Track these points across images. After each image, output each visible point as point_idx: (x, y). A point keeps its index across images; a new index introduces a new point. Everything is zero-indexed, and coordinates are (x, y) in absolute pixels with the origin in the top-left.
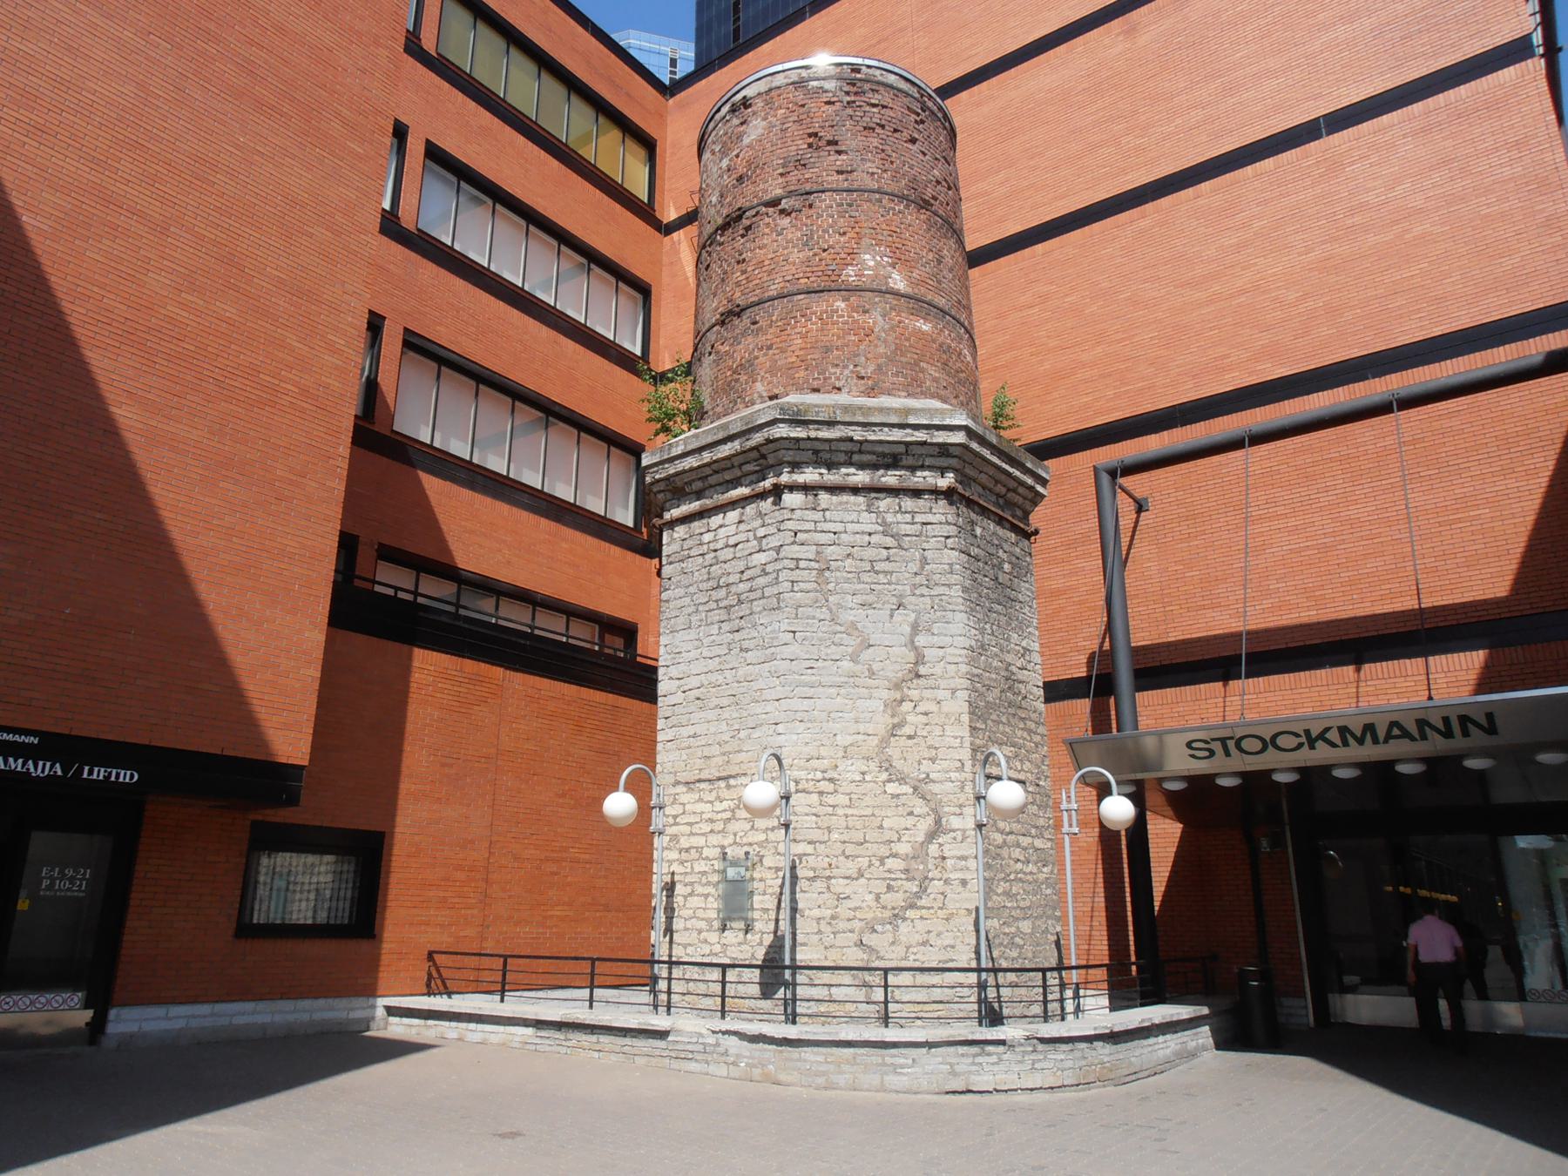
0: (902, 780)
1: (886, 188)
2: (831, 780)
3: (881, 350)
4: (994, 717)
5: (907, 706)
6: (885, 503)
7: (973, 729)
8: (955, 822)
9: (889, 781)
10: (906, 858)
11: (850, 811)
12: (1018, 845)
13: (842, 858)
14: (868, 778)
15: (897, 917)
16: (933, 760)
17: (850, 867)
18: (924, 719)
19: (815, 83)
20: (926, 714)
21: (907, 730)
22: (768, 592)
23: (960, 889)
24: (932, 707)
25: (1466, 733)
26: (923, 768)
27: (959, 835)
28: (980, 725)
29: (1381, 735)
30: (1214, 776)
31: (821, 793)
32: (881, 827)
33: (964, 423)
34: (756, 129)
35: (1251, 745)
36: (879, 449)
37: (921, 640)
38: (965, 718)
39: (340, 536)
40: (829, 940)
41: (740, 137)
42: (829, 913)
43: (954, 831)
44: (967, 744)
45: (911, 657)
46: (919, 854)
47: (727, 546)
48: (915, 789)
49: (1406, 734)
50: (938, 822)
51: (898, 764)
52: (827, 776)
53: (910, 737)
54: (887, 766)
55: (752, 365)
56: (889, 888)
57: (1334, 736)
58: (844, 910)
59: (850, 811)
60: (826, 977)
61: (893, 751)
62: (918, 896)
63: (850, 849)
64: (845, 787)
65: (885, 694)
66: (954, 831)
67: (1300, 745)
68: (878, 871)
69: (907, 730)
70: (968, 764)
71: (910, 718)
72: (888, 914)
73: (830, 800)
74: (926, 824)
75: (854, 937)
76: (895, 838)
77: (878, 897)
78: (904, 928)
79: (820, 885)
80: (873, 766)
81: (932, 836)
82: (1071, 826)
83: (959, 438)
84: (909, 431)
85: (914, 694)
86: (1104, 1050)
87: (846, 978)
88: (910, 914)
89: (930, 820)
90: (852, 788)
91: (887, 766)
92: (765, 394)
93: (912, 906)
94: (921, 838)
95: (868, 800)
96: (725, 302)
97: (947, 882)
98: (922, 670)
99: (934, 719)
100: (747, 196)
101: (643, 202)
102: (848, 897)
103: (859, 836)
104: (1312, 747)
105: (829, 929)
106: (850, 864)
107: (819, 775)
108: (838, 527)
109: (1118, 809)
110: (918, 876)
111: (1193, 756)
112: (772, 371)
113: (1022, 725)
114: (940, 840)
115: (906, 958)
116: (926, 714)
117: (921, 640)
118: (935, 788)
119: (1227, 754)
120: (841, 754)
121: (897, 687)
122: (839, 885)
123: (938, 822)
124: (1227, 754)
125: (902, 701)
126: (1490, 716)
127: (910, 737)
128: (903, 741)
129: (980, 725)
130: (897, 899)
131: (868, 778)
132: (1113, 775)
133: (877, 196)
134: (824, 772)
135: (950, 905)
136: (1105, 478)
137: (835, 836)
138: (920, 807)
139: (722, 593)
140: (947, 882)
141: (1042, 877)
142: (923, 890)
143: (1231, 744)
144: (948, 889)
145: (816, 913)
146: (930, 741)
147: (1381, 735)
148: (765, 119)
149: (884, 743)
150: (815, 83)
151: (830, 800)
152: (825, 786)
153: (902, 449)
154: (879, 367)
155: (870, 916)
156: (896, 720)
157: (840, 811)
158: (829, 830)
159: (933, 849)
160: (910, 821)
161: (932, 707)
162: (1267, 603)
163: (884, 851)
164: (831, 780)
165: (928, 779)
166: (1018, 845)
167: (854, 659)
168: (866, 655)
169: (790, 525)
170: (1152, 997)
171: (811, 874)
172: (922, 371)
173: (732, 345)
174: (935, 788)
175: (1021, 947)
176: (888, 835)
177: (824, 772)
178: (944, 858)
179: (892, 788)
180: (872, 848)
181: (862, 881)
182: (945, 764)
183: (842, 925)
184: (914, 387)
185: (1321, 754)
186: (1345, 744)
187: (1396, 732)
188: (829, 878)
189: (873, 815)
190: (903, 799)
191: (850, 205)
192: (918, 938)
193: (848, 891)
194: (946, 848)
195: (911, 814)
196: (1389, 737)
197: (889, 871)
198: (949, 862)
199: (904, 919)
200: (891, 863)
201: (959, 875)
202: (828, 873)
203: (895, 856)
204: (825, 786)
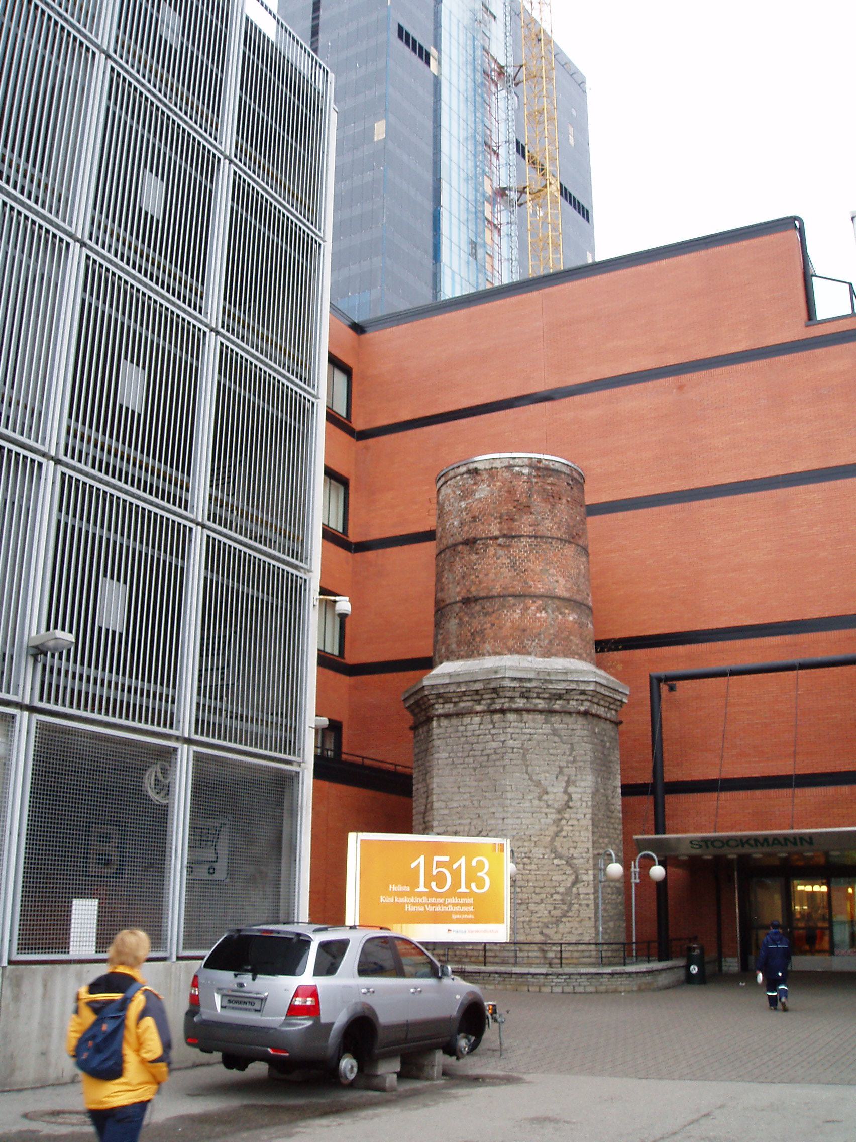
0: (561, 858)
1: (554, 536)
2: (529, 858)
3: (551, 632)
4: (601, 825)
5: (564, 822)
6: (555, 719)
7: (593, 833)
8: (585, 877)
9: (555, 858)
10: (562, 894)
11: (537, 872)
12: (609, 886)
13: (534, 895)
14: (545, 857)
15: (558, 921)
16: (575, 848)
17: (537, 898)
18: (570, 828)
19: (517, 469)
20: (572, 826)
21: (564, 834)
22: (498, 763)
23: (586, 908)
24: (576, 823)
25: (802, 844)
26: (570, 852)
27: (586, 883)
28: (596, 830)
29: (770, 842)
30: (702, 855)
31: (524, 864)
32: (551, 880)
33: (594, 680)
34: (483, 491)
35: (718, 844)
36: (551, 691)
37: (570, 789)
38: (590, 828)
39: (412, 791)
40: (528, 931)
41: (473, 492)
42: (528, 919)
43: (584, 881)
44: (590, 840)
45: (566, 797)
46: (568, 891)
47: (473, 735)
48: (567, 862)
49: (779, 843)
50: (577, 877)
51: (559, 850)
52: (527, 855)
53: (564, 837)
54: (554, 851)
55: (482, 633)
56: (555, 908)
57: (752, 842)
58: (534, 919)
59: (537, 872)
60: (526, 947)
61: (557, 844)
62: (567, 912)
63: (537, 890)
64: (535, 861)
65: (554, 816)
66: (584, 881)
67: (738, 846)
68: (550, 900)
69: (564, 834)
70: (591, 850)
71: (565, 828)
72: (554, 920)
73: (529, 867)
74: (571, 879)
75: (538, 930)
76: (558, 885)
77: (550, 912)
78: (561, 926)
79: (524, 907)
80: (548, 851)
81: (574, 883)
82: (635, 878)
83: (591, 687)
84: (568, 683)
85: (567, 816)
86: (649, 978)
87: (535, 947)
88: (563, 919)
89: (573, 877)
90: (539, 861)
91: (554, 851)
92: (491, 651)
93: (565, 916)
94: (569, 885)
95: (546, 867)
96: (465, 591)
97: (580, 905)
98: (571, 804)
99: (576, 828)
100: (480, 530)
101: (342, 417)
102: (536, 912)
103: (541, 884)
104: (743, 846)
105: (528, 927)
106: (537, 897)
107: (523, 855)
108: (532, 731)
109: (657, 871)
110: (568, 902)
111: (692, 848)
112: (495, 639)
113: (612, 827)
114: (578, 886)
115: (562, 939)
116: (572, 826)
117: (570, 789)
118: (576, 861)
119: (707, 847)
120: (533, 845)
121: (559, 812)
122: (532, 906)
123: (577, 877)
124: (707, 847)
125: (561, 819)
126: (810, 838)
127: (564, 837)
128: (561, 839)
129: (596, 830)
130: (557, 913)
131: (545, 857)
132: (653, 852)
133: (550, 540)
134: (526, 853)
135: (582, 915)
136: (655, 681)
137: (531, 884)
138: (569, 871)
139: (471, 760)
140: (580, 905)
141: (618, 901)
142: (570, 909)
143: (709, 843)
144: (581, 908)
145: (522, 919)
146: (574, 839)
147: (770, 842)
148: (489, 486)
149: (553, 839)
150: (517, 469)
151: (529, 867)
152: (526, 860)
153: (564, 691)
154: (550, 641)
155: (546, 920)
156: (558, 829)
157: (533, 872)
158: (528, 881)
159: (574, 890)
160: (564, 877)
161: (576, 823)
162: (734, 752)
163: (553, 891)
164: (529, 858)
165: (572, 857)
166: (609, 886)
167: (540, 799)
168: (545, 797)
169: (509, 730)
170: (667, 958)
171: (520, 901)
172: (571, 641)
173: (470, 618)
174: (576, 861)
175: (609, 934)
176: (554, 884)
177: (526, 853)
178: (579, 894)
179: (556, 861)
180: (548, 890)
181: (543, 905)
182: (580, 850)
183: (534, 925)
184: (567, 653)
185: (746, 850)
186: (756, 846)
187: (776, 842)
188: (528, 903)
189: (548, 874)
190: (561, 867)
191: (536, 546)
192: (567, 930)
193: (536, 909)
194: (580, 889)
195: (565, 873)
196: (773, 844)
197: (555, 900)
198: (582, 896)
199: (561, 922)
200: (556, 897)
201: (586, 902)
202: (527, 901)
203: (558, 893)
204: (526, 860)
